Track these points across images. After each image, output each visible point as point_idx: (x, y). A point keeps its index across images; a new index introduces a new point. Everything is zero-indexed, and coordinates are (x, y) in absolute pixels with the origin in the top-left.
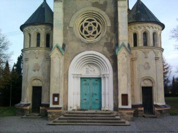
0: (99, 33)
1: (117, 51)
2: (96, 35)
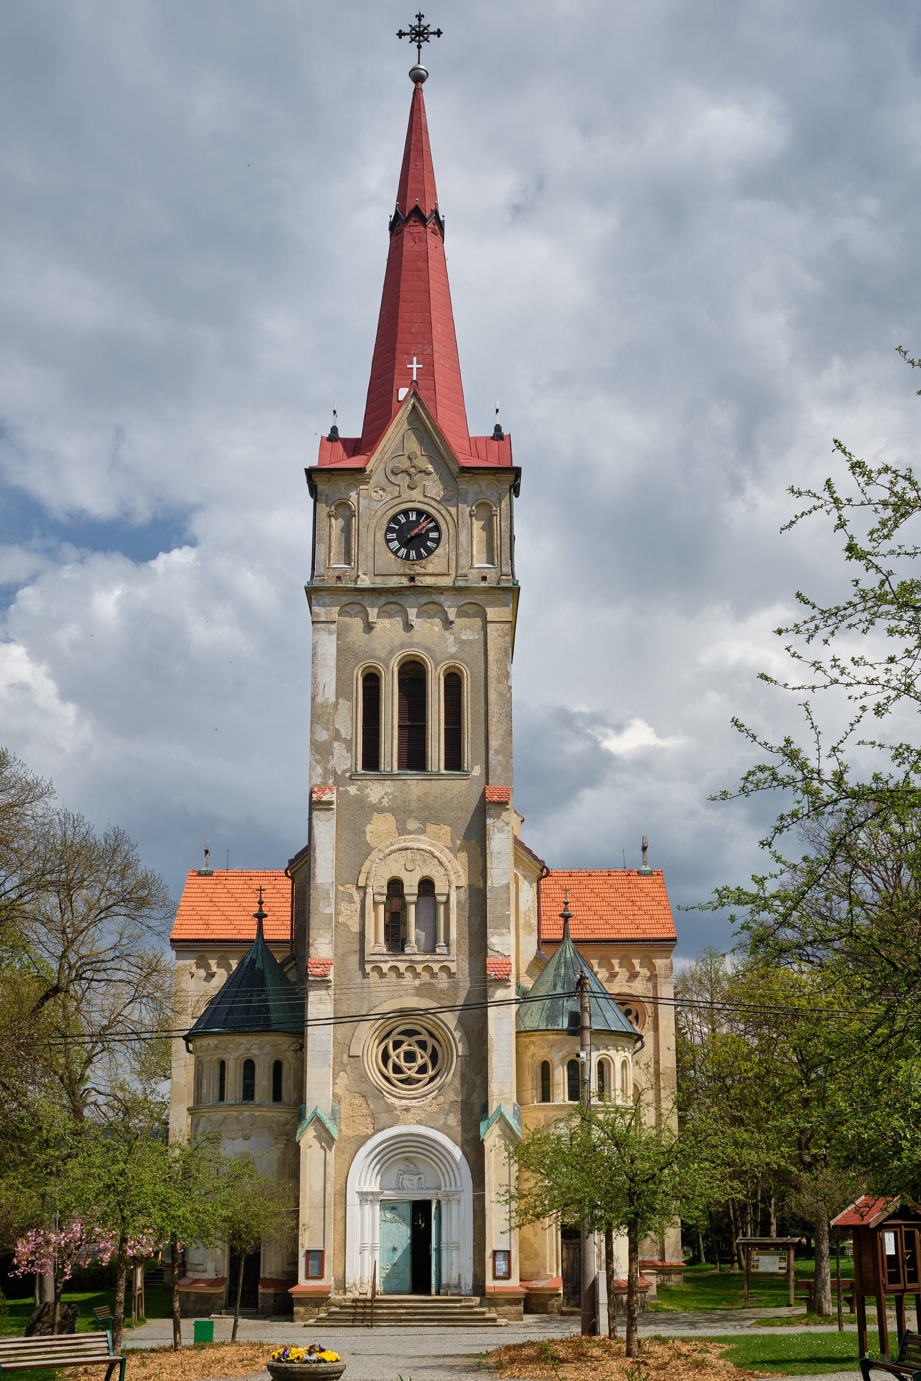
0: (424, 1031)
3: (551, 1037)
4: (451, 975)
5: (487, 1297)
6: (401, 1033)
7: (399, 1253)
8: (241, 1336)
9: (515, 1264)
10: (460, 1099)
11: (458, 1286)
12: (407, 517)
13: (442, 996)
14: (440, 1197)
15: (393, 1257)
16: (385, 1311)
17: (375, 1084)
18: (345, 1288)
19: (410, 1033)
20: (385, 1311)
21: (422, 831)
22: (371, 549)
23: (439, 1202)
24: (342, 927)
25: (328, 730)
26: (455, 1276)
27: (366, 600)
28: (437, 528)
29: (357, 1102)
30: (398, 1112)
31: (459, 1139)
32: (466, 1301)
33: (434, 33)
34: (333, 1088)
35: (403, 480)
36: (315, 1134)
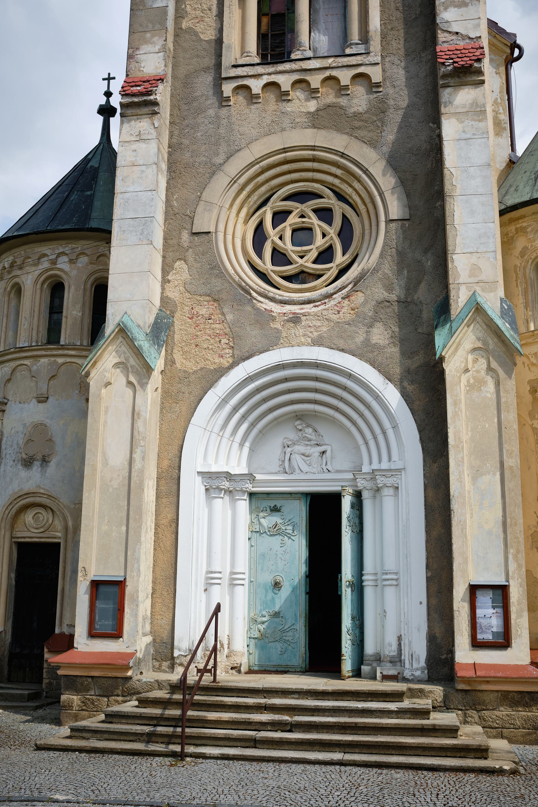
0: (348, 257)
1: (439, 338)
2: (333, 268)
5: (461, 686)
6: (288, 198)
7: (285, 592)
9: (519, 616)
10: (393, 297)
13: (357, 124)
14: (361, 484)
15: (273, 599)
16: (226, 716)
17: (237, 278)
18: (173, 658)
20: (226, 716)
23: (358, 496)
24: (187, 36)
26: (391, 639)
29: (203, 311)
30: (278, 325)
31: (397, 370)
32: (413, 694)
34: (163, 289)
36: (117, 360)
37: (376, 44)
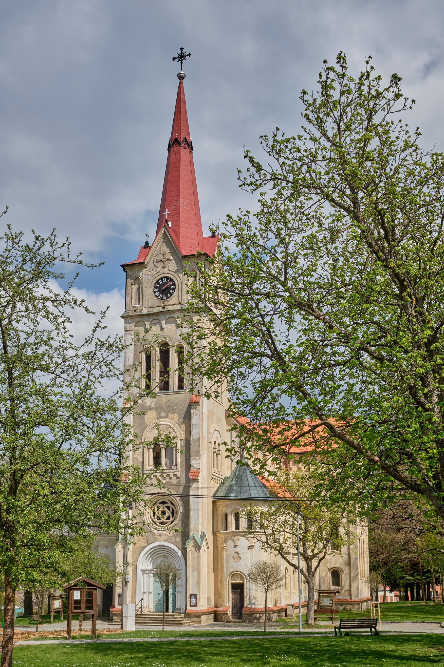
0: (169, 502)
3: (226, 502)
4: (178, 478)
8: (39, 629)
11: (180, 609)
12: (162, 281)
19: (163, 503)
21: (167, 417)
22: (147, 297)
25: (130, 376)
26: (179, 605)
27: (145, 319)
28: (174, 284)
31: (181, 548)
33: (188, 55)
35: (161, 265)
37: (179, 466)
